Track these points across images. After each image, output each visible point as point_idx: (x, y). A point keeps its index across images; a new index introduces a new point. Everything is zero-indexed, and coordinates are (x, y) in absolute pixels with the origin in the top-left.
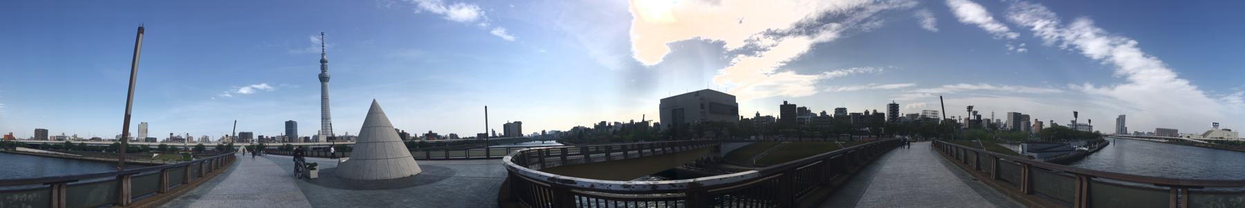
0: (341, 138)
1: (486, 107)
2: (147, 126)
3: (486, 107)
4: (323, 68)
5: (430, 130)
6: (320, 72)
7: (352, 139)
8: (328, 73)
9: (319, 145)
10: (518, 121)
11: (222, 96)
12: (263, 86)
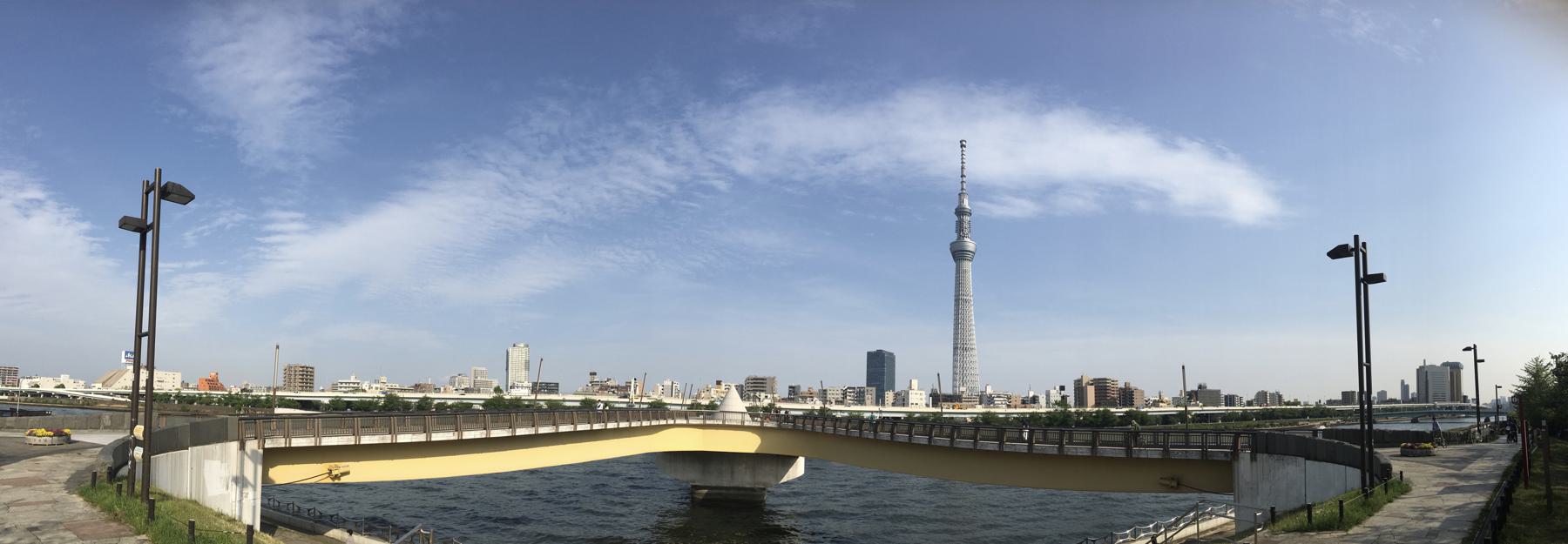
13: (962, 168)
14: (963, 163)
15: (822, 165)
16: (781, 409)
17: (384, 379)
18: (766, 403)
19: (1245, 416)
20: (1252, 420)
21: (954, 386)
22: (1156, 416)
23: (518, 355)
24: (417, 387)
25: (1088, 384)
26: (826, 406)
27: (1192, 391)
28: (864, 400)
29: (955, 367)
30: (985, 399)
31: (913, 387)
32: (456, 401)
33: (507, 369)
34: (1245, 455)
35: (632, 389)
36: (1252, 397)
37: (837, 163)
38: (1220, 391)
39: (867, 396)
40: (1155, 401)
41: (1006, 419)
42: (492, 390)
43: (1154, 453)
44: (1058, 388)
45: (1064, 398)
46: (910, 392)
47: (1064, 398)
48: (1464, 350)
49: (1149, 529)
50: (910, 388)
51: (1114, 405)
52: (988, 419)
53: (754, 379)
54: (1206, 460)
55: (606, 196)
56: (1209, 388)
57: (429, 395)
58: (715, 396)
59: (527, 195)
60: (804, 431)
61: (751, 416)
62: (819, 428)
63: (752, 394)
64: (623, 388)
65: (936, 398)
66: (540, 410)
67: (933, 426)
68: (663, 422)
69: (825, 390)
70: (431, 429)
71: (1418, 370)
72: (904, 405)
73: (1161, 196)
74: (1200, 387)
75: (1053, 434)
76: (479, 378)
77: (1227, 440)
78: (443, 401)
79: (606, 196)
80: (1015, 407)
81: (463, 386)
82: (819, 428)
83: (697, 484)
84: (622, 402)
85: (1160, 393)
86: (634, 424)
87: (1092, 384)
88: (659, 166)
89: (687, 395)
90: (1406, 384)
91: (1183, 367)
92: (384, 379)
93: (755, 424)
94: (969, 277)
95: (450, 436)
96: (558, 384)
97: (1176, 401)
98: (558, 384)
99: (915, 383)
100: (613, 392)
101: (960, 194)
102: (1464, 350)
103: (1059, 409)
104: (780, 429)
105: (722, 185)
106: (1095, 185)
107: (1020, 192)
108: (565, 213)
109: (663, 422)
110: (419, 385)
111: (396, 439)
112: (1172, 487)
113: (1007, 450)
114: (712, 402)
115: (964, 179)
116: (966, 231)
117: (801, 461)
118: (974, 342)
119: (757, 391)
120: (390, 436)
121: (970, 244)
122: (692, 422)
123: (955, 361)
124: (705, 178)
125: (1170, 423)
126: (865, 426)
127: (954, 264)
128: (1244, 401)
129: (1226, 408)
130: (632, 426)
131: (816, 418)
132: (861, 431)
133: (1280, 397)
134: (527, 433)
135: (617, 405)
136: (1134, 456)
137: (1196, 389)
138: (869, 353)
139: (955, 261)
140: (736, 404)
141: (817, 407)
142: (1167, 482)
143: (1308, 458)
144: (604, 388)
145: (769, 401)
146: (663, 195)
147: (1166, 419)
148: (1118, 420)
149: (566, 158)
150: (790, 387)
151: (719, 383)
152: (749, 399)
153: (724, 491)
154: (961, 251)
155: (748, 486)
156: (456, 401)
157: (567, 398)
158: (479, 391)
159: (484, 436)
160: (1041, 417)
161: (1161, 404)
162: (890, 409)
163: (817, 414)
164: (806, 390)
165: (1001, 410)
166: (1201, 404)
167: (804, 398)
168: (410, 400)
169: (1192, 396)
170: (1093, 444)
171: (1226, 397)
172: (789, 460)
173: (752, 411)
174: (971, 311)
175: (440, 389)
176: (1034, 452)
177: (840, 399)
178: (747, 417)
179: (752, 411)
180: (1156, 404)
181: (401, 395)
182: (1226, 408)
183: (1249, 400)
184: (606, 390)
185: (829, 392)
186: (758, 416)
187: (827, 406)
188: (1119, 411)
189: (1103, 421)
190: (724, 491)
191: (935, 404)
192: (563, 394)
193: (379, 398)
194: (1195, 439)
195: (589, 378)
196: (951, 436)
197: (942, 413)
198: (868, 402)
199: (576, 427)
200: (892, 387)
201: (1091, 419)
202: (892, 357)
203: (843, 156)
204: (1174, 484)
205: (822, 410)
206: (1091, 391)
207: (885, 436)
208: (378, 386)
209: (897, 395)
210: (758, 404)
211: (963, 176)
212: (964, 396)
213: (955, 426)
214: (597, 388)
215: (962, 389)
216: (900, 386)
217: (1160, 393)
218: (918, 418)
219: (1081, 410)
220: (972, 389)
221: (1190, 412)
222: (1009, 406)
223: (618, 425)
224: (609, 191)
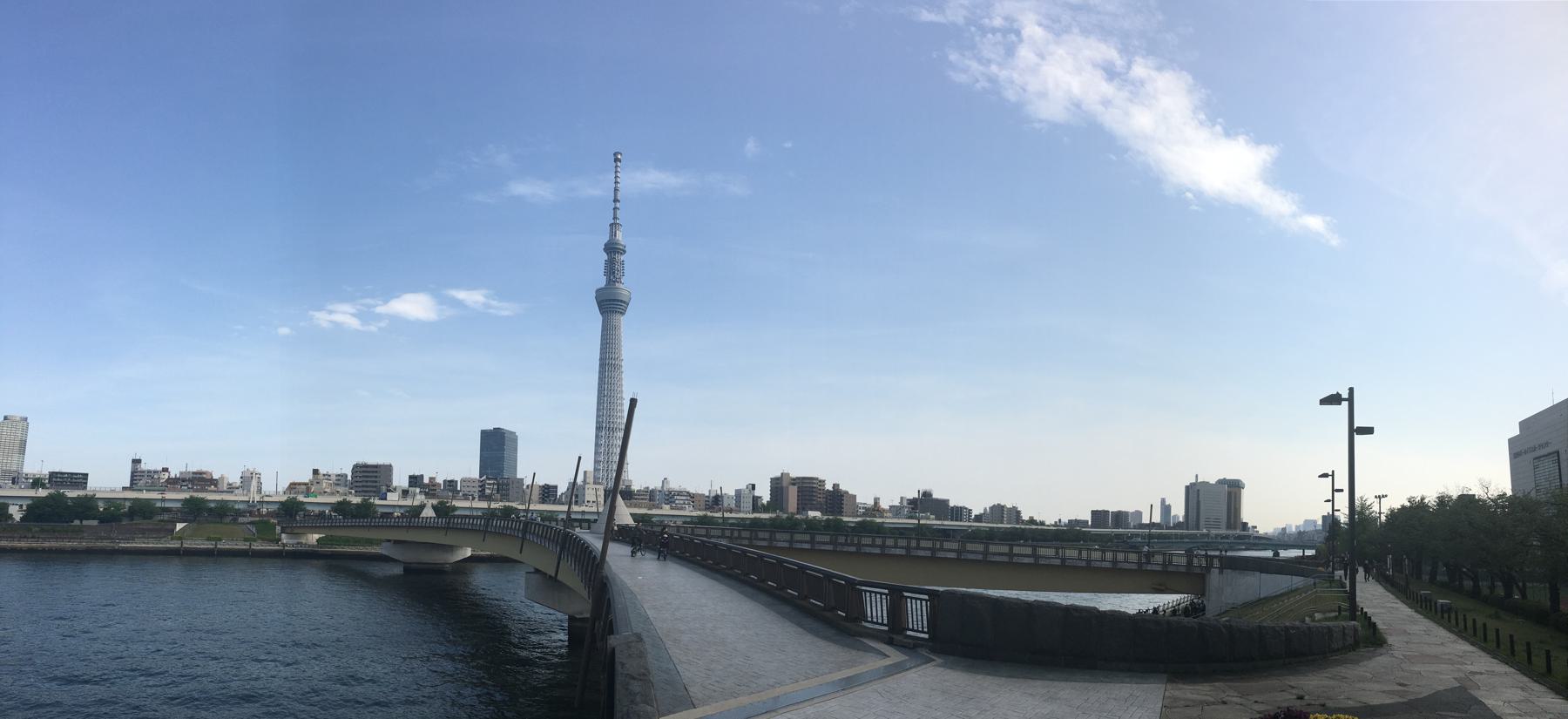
0: (650, 496)
1: (580, 458)
2: (25, 430)
3: (580, 458)
4: (612, 270)
5: (924, 487)
6: (602, 282)
7: (679, 500)
8: (628, 285)
9: (583, 512)
10: (1230, 476)
11: (322, 318)
12: (473, 297)
13: (616, 190)
14: (616, 182)
19: (974, 536)
31: (588, 481)
34: (1215, 572)
48: (1319, 477)
56: (934, 496)
71: (1187, 487)
87: (794, 484)
90: (1167, 503)
96: (87, 475)
98: (87, 475)
101: (611, 225)
102: (1319, 477)
115: (618, 205)
127: (598, 318)
133: (1018, 513)
138: (483, 432)
143: (1261, 572)
154: (614, 300)
166: (933, 517)
202: (513, 438)
211: (616, 200)
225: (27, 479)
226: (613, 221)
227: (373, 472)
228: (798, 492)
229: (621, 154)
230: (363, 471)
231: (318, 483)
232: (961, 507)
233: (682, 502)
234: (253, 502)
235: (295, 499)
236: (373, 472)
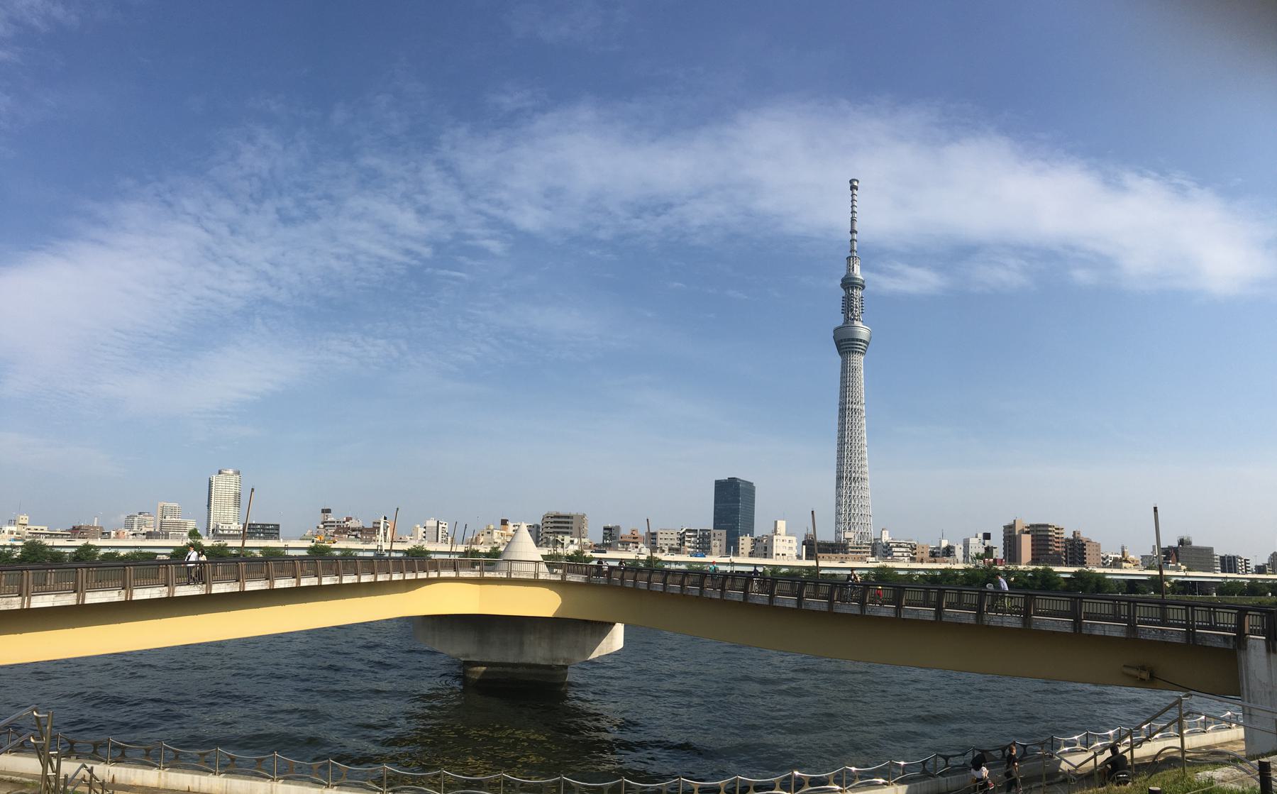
13: (853, 220)
14: (853, 212)
15: (637, 218)
16: (592, 559)
17: (24, 519)
18: (571, 550)
20: (1265, 594)
21: (838, 532)
22: (1117, 580)
23: (225, 486)
24: (76, 531)
25: (1022, 532)
26: (655, 555)
27: (1170, 548)
28: (709, 548)
29: (838, 504)
30: (879, 549)
32: (133, 550)
33: (209, 505)
35: (382, 531)
36: (1263, 560)
37: (658, 215)
38: (1212, 549)
39: (713, 542)
40: (1115, 560)
41: (909, 577)
42: (186, 534)
43: (1115, 630)
44: (980, 536)
45: (989, 550)
46: (775, 537)
47: (989, 550)
49: (1107, 737)
50: (775, 532)
51: (1059, 564)
52: (883, 576)
53: (555, 517)
54: (1192, 646)
55: (334, 263)
56: (1194, 544)
57: (91, 542)
58: (499, 541)
59: (238, 262)
60: (622, 588)
61: (548, 566)
62: (643, 584)
63: (552, 538)
64: (368, 530)
65: (812, 547)
66: (254, 560)
67: (804, 583)
68: (422, 575)
69: (655, 534)
70: (84, 588)
72: (765, 556)
73: (1103, 263)
74: (1182, 542)
75: (970, 598)
76: (168, 518)
77: (1227, 618)
78: (113, 551)
79: (334, 263)
80: (922, 561)
81: (145, 530)
82: (643, 584)
83: (472, 659)
84: (367, 550)
85: (1123, 548)
86: (381, 578)
87: (1028, 533)
88: (407, 221)
89: (459, 537)
91: (1155, 509)
92: (24, 519)
93: (553, 578)
94: (861, 377)
95: (114, 596)
96: (278, 525)
97: (1147, 562)
98: (278, 525)
99: (782, 525)
100: (356, 536)
101: (849, 258)
103: (981, 563)
104: (587, 584)
105: (495, 246)
106: (1021, 250)
107: (917, 255)
108: (280, 288)
109: (422, 575)
110: (79, 528)
111: (29, 602)
112: (1142, 680)
113: (907, 617)
114: (495, 549)
115: (855, 236)
116: (857, 312)
117: (619, 630)
118: (867, 469)
119: (558, 533)
120: (19, 599)
121: (862, 331)
122: (463, 574)
123: (839, 495)
124: (471, 237)
125: (1136, 592)
126: (708, 582)
127: (838, 359)
128: (1252, 566)
129: (1224, 575)
130: (379, 580)
131: (640, 570)
132: (702, 588)
134: (228, 591)
135: (361, 554)
136: (1084, 632)
137: (1176, 544)
139: (841, 354)
140: (528, 551)
141: (643, 557)
142: (1134, 672)
144: (342, 530)
145: (576, 548)
146: (414, 262)
147: (1132, 585)
148: (1064, 584)
149: (278, 211)
150: (605, 529)
151: (504, 522)
152: (547, 544)
153: (509, 669)
154: (849, 340)
155: (543, 663)
156: (133, 550)
157: (291, 544)
158: (167, 536)
159: (164, 595)
160: (957, 576)
161: (1124, 564)
162: (744, 561)
163: (642, 565)
164: (629, 533)
165: (902, 564)
166: (1183, 567)
167: (625, 544)
168: (62, 550)
169: (1170, 555)
170: (1026, 614)
171: (1222, 558)
172: (603, 628)
173: (551, 562)
174: (863, 426)
175: (109, 534)
176: (944, 619)
177: (676, 546)
178: (543, 567)
179: (551, 562)
180: (1117, 563)
181: (49, 542)
182: (1224, 575)
183: (1260, 564)
184: (345, 533)
185: (660, 536)
186: (560, 567)
187: (658, 555)
188: (1065, 571)
189: (1045, 583)
190: (509, 669)
191: (810, 555)
192: (286, 539)
193: (13, 547)
194: (1176, 614)
195: (321, 517)
196: (830, 597)
197: (817, 568)
198: (715, 550)
199: (299, 582)
200: (749, 530)
201: (1026, 580)
202: (750, 488)
203: (669, 206)
204: (1145, 675)
205: (650, 560)
206: (1026, 542)
207: (737, 595)
208: (14, 528)
209: (756, 541)
210: (560, 551)
211: (853, 231)
212: (851, 544)
213: (837, 585)
214: (331, 531)
215: (848, 535)
216: (760, 529)
217: (1123, 548)
218: (786, 574)
219: (1012, 567)
220: (862, 535)
221: (1167, 578)
222: (913, 560)
223: (359, 579)
224: (338, 257)
225: (223, 530)
226: (850, 254)
227: (565, 522)
228: (1032, 541)
229: (858, 181)
230: (555, 522)
231: (489, 533)
232: (1234, 557)
233: (900, 554)
234: (381, 550)
235: (1048, 572)
236: (565, 522)
